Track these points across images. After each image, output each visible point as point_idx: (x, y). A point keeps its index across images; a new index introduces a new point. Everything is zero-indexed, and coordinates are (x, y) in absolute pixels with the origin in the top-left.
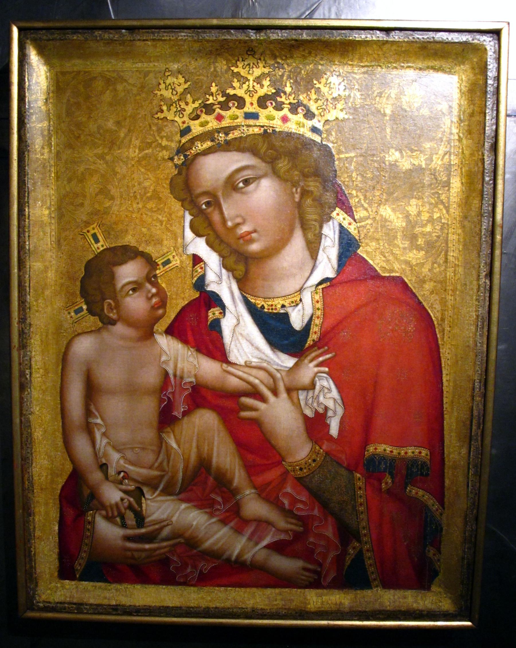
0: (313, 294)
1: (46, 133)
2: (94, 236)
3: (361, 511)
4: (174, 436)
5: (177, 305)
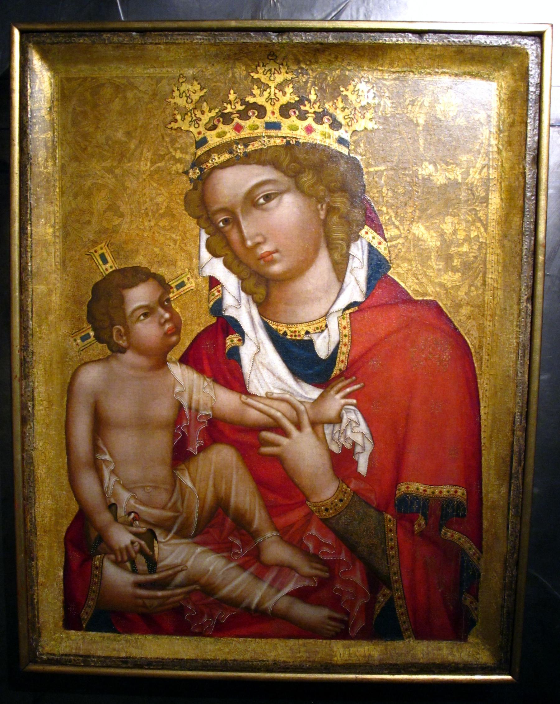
0: (339, 319)
1: (50, 144)
2: (103, 256)
3: (391, 555)
4: (189, 473)
5: (192, 331)
